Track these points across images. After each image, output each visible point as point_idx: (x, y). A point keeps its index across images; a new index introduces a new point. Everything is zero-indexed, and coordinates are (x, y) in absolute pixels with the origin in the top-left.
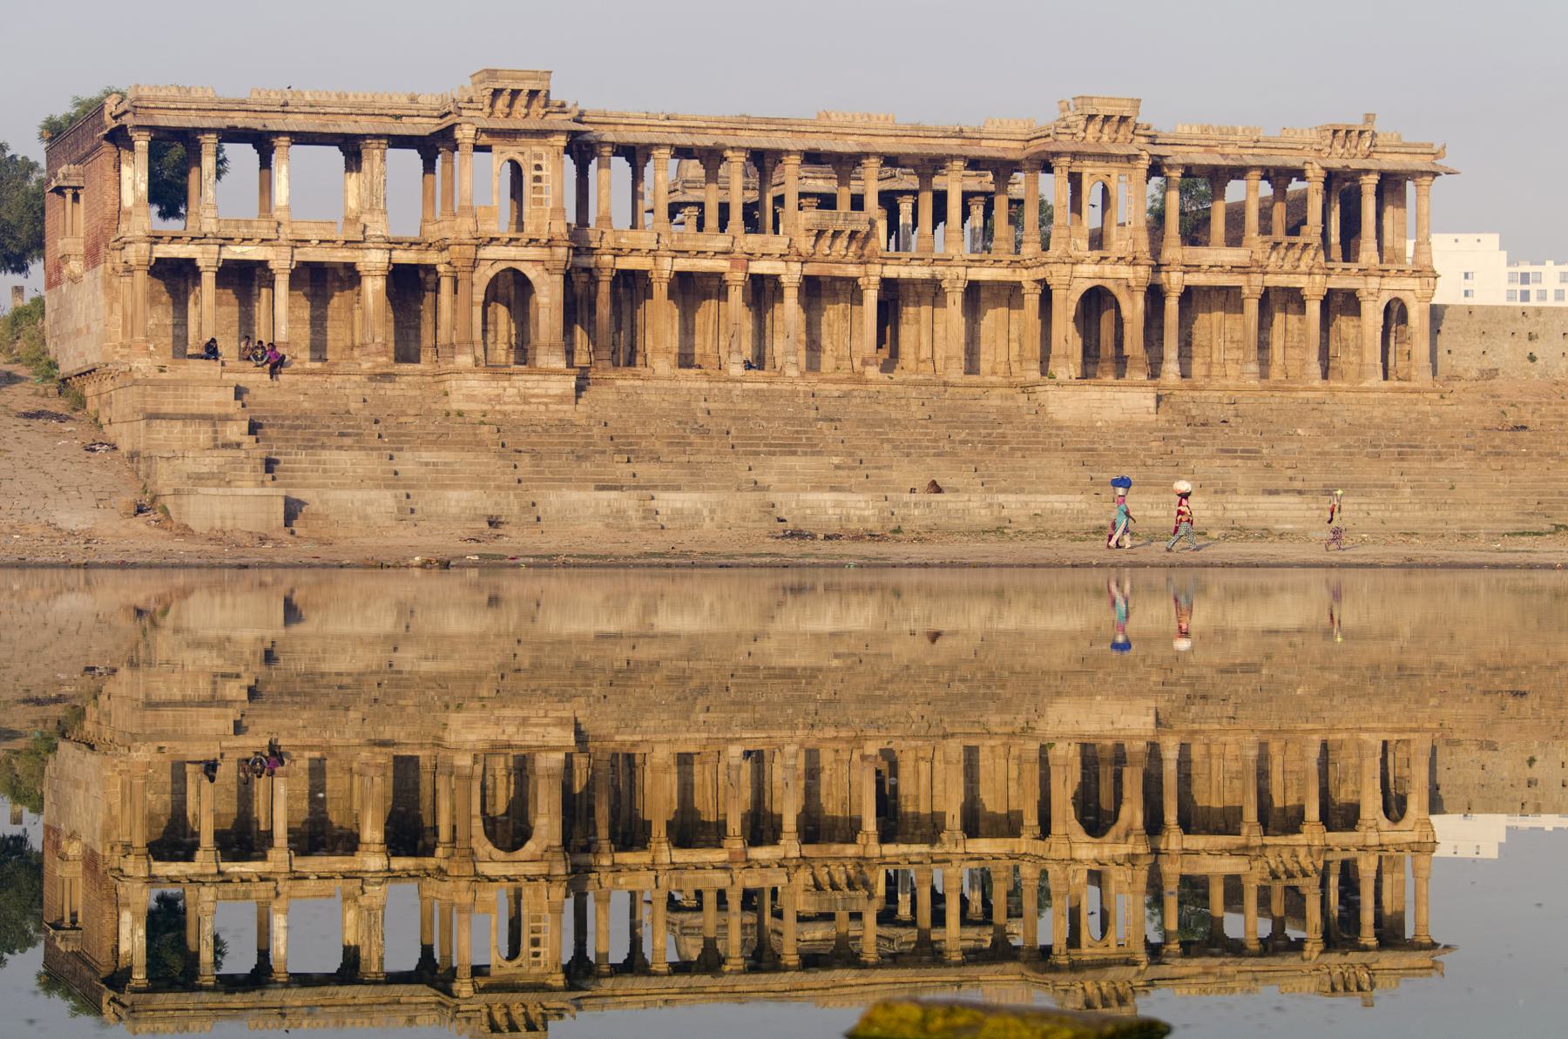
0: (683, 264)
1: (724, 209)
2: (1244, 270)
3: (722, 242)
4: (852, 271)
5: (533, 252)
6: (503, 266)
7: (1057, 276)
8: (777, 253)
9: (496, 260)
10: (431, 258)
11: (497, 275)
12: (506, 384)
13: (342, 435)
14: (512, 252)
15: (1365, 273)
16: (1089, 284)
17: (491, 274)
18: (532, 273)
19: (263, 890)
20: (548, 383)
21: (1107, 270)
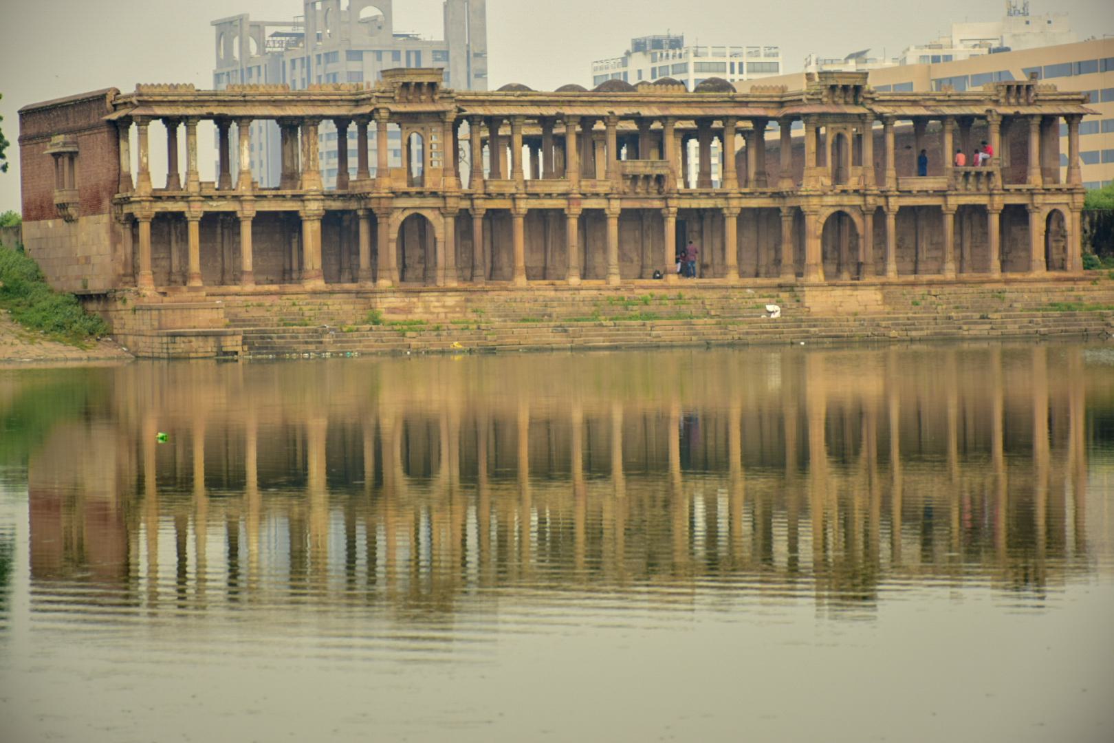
0: (535, 204)
1: (741, 64)
2: (942, 193)
3: (560, 187)
4: (657, 204)
5: (431, 202)
6: (407, 213)
7: (807, 205)
8: (14, 239)
9: (405, 209)
10: (353, 205)
11: (406, 219)
12: (415, 300)
13: (307, 343)
14: (417, 202)
15: (1031, 193)
16: (832, 210)
17: (402, 218)
18: (430, 215)
19: (492, 189)
20: (391, 408)
21: (846, 200)
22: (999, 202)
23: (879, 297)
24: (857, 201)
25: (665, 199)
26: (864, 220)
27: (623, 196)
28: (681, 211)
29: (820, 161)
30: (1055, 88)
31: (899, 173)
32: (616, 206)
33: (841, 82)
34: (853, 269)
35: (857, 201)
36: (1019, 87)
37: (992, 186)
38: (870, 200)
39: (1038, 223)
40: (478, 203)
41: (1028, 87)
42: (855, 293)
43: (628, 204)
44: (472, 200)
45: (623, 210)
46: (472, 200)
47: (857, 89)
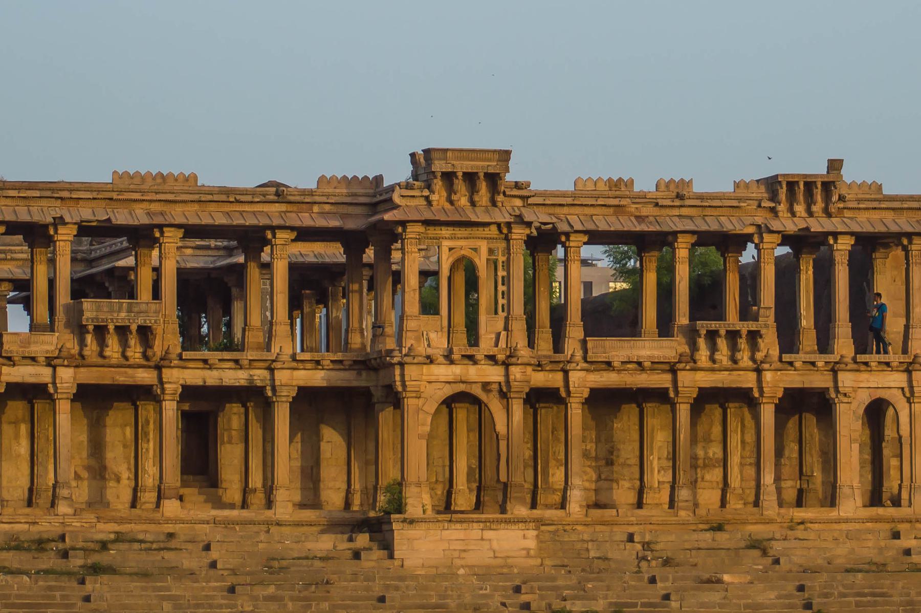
21: (473, 373)
22: (776, 382)
23: (531, 544)
24: (495, 374)
25: (158, 368)
26: (508, 409)
27: (79, 361)
28: (189, 392)
29: (503, 311)
30: (880, 188)
31: (588, 332)
32: (67, 377)
33: (462, 166)
34: (388, 510)
35: (495, 374)
36: (809, 186)
37: (759, 356)
38: (516, 372)
39: (849, 422)
40: (282, 376)
41: (827, 187)
42: (488, 534)
43: (89, 376)
44: (271, 370)
45: (80, 386)
46: (271, 370)
47: (493, 179)
